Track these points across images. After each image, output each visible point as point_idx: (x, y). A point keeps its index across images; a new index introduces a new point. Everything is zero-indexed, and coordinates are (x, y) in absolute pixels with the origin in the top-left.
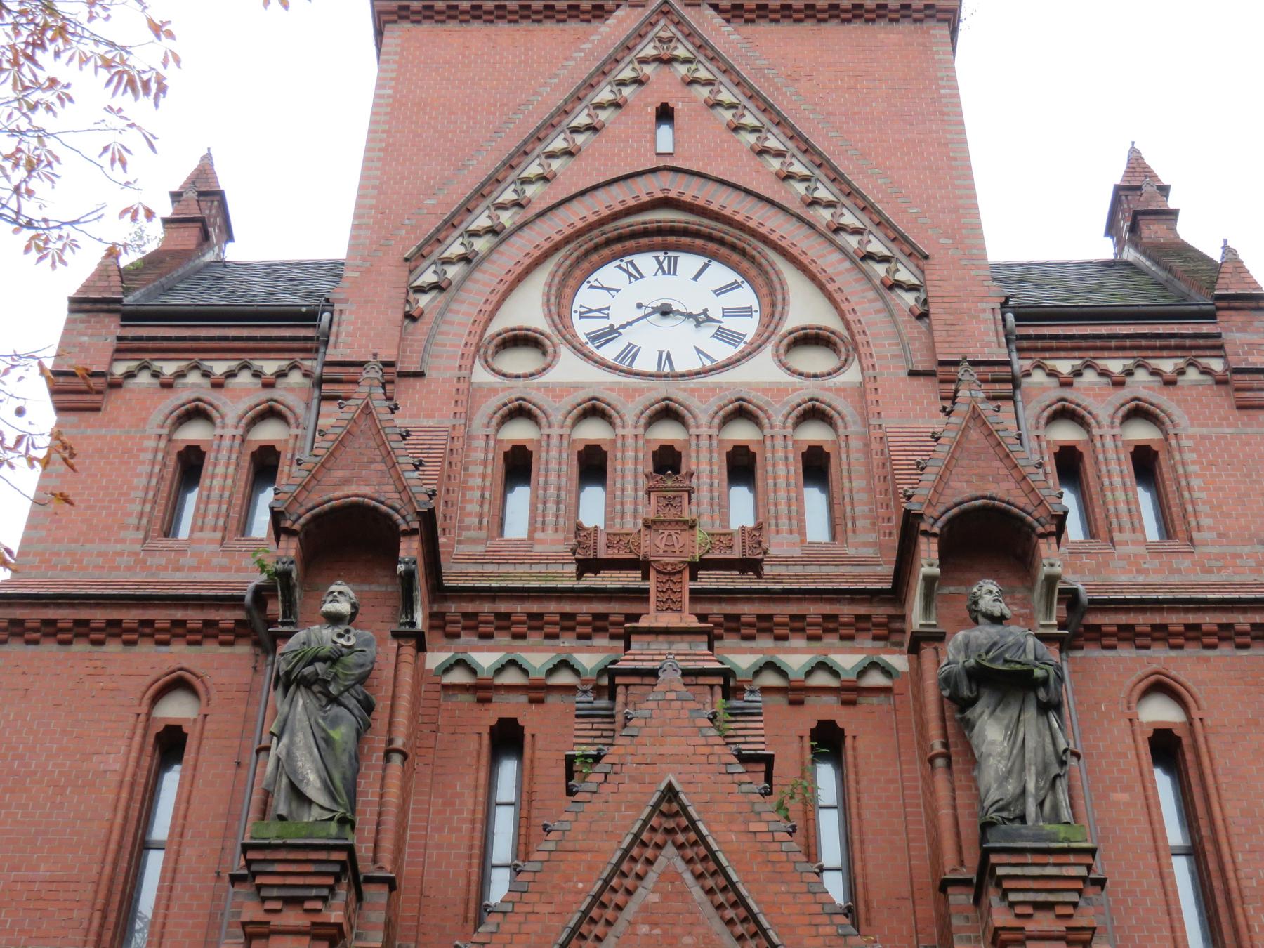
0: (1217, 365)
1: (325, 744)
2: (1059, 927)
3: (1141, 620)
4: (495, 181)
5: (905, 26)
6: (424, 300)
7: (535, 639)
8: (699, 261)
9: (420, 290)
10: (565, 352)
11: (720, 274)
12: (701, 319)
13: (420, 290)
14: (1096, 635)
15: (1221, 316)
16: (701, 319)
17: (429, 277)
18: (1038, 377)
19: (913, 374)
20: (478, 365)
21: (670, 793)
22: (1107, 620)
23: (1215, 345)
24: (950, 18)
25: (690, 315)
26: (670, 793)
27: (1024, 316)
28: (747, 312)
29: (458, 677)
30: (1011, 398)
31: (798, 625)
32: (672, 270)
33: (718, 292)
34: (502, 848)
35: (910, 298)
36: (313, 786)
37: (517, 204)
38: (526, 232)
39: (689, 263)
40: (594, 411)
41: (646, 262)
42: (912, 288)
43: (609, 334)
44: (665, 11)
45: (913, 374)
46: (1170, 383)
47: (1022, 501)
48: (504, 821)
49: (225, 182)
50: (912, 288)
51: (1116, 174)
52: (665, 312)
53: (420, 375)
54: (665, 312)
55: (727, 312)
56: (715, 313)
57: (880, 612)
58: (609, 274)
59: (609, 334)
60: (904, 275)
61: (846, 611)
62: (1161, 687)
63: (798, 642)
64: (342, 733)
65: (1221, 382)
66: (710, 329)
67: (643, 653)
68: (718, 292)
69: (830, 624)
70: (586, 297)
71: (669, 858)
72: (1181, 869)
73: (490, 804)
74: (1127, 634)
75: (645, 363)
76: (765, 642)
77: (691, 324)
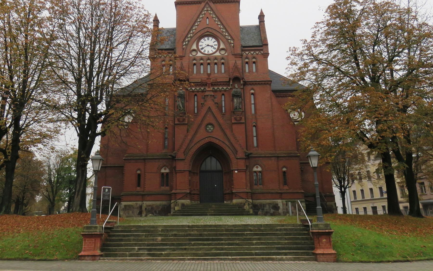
0: (262, 52)
1: (182, 103)
3: (251, 83)
5: (234, 3)
6: (184, 46)
7: (197, 86)
8: (212, 38)
9: (184, 45)
10: (199, 52)
11: (214, 40)
12: (212, 46)
13: (184, 45)
14: (247, 84)
16: (212, 46)
18: (245, 54)
22: (248, 83)
23: (262, 50)
24: (239, 2)
25: (211, 46)
27: (244, 47)
28: (216, 45)
29: (191, 90)
30: (242, 57)
31: (221, 84)
32: (209, 40)
33: (214, 42)
34: (196, 105)
38: (195, 36)
39: (210, 38)
41: (206, 38)
42: (232, 43)
43: (202, 48)
44: (207, 3)
47: (240, 76)
48: (196, 103)
50: (232, 43)
51: (259, 14)
52: (208, 45)
54: (208, 45)
55: (214, 45)
56: (213, 46)
57: (228, 83)
58: (202, 40)
59: (202, 48)
60: (232, 42)
61: (225, 83)
62: (252, 89)
66: (213, 47)
67: (207, 93)
68: (214, 42)
69: (223, 84)
70: (200, 44)
71: (210, 113)
72: (253, 106)
74: (250, 84)
75: (206, 53)
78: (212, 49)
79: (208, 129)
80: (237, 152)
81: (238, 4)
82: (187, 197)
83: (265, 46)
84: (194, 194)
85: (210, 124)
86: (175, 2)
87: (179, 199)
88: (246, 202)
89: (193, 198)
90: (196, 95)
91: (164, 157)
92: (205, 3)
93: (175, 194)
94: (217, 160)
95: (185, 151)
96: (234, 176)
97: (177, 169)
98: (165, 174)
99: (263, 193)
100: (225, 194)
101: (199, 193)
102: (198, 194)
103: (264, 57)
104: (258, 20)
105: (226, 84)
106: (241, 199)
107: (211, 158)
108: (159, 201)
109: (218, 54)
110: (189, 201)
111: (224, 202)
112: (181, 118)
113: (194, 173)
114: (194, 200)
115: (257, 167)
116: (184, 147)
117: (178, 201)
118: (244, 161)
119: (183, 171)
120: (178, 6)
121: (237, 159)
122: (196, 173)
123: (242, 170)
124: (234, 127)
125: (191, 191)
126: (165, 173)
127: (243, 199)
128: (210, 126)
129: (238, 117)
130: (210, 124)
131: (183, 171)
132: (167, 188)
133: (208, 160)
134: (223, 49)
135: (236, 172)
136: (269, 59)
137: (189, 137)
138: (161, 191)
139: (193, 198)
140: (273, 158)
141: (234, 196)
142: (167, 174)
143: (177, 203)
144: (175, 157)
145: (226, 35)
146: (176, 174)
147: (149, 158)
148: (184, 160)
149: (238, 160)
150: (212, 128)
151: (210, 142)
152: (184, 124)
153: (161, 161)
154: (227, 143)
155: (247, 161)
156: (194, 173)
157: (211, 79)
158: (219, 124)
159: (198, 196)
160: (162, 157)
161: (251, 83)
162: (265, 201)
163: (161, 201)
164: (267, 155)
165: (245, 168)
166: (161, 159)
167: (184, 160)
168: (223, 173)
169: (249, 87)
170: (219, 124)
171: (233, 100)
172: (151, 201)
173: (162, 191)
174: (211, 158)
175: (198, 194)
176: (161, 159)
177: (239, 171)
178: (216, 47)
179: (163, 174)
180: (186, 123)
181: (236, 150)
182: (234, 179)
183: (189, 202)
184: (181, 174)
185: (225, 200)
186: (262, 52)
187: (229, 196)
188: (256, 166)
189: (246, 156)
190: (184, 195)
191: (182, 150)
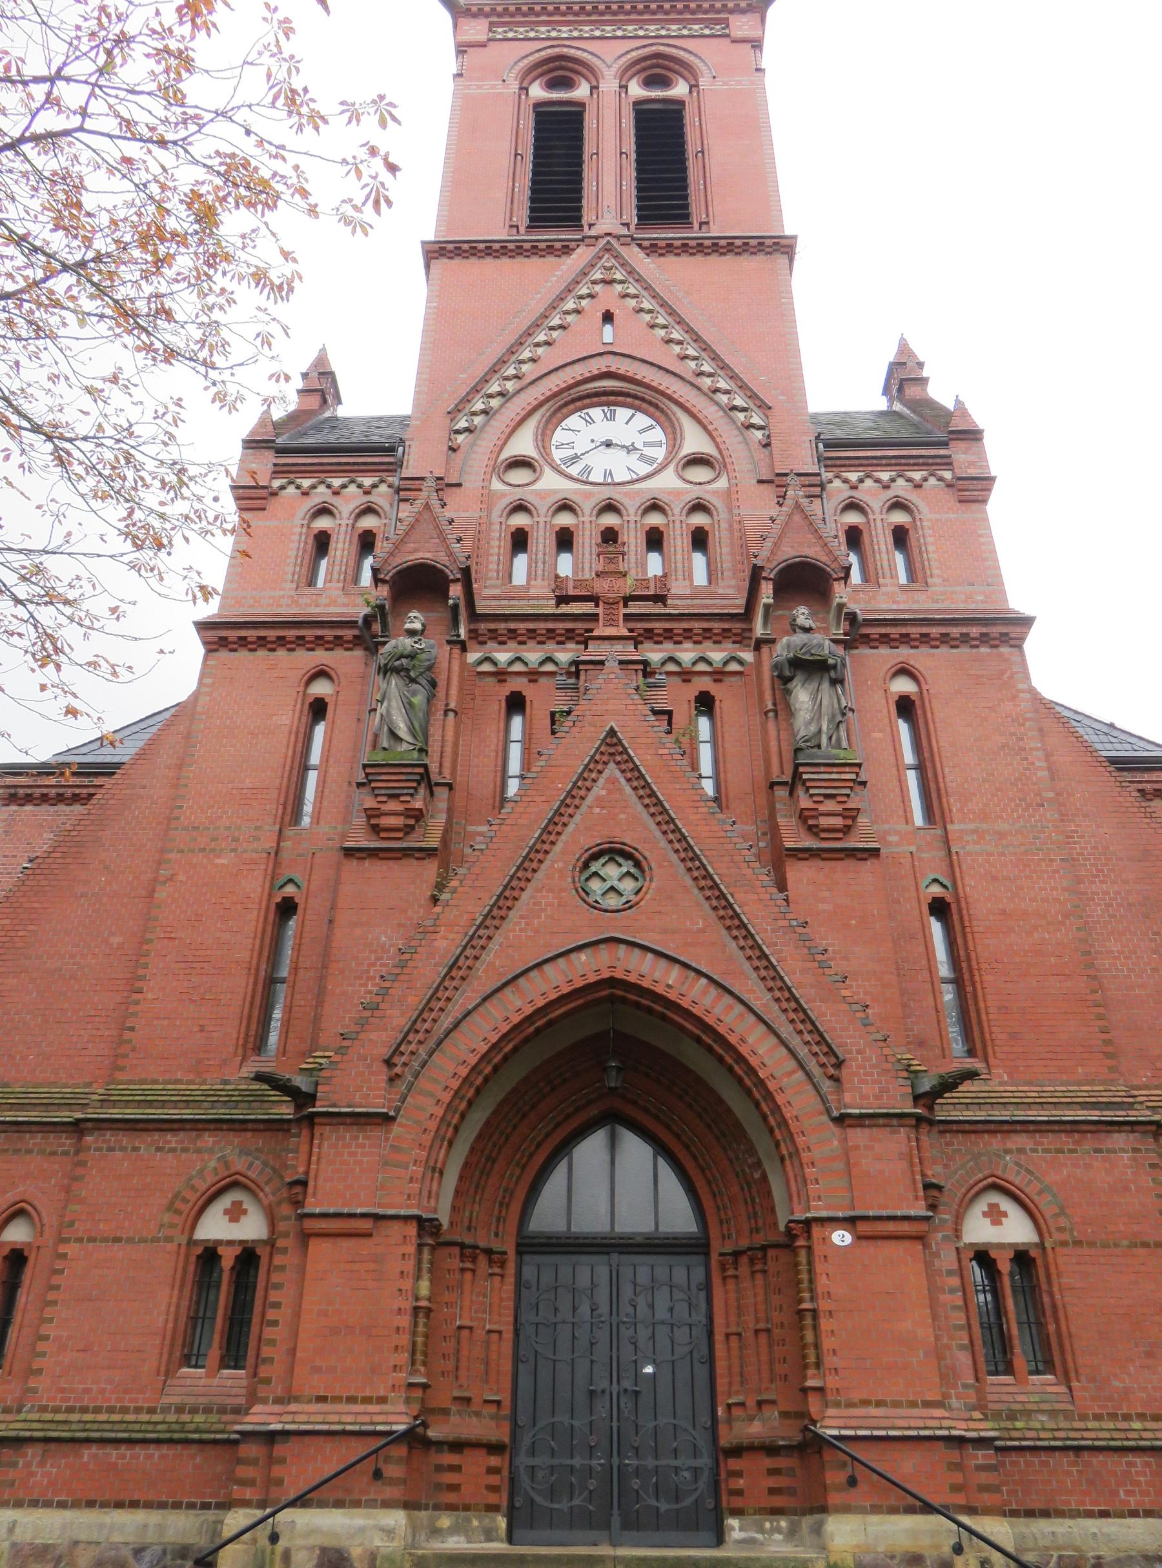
0: (948, 475)
1: (409, 706)
2: (838, 808)
3: (894, 631)
4: (502, 362)
6: (460, 438)
7: (531, 644)
9: (458, 432)
10: (547, 470)
11: (642, 420)
12: (631, 449)
13: (458, 432)
14: (866, 640)
15: (952, 444)
16: (631, 449)
17: (462, 424)
18: (837, 483)
19: (760, 482)
20: (494, 479)
21: (612, 732)
23: (947, 463)
25: (623, 447)
26: (612, 732)
29: (486, 667)
31: (688, 634)
33: (641, 432)
35: (759, 434)
36: (402, 731)
37: (516, 377)
38: (522, 395)
39: (623, 413)
40: (565, 506)
41: (596, 413)
45: (760, 482)
46: (918, 486)
47: (824, 559)
49: (335, 367)
51: (890, 355)
52: (608, 444)
53: (459, 485)
54: (608, 444)
56: (639, 445)
57: (737, 626)
58: (574, 421)
60: (756, 420)
62: (904, 671)
63: (688, 645)
64: (419, 700)
65: (949, 486)
66: (635, 456)
68: (641, 432)
70: (559, 436)
71: (612, 770)
72: (912, 777)
73: (506, 741)
74: (885, 640)
76: (668, 645)
77: (623, 453)
78: (633, 460)
79: (596, 886)
80: (839, 1065)
81: (783, 260)
82: (377, 1474)
83: (962, 445)
84: (457, 1446)
85: (615, 852)
86: (424, 243)
87: (301, 1501)
88: (958, 1549)
89: (454, 1488)
90: (516, 704)
91: (237, 1114)
92: (592, 252)
93: (271, 1437)
94: (662, 1148)
95: (397, 1051)
96: (822, 1282)
97: (313, 1206)
98: (228, 1258)
99: (1078, 1449)
100: (736, 1451)
101: (500, 1433)
102: (494, 1448)
103: (960, 501)
104: (884, 399)
105: (726, 633)
106: (910, 1510)
107: (613, 1144)
108: (134, 1505)
109: (668, 481)
110: (397, 1518)
111: (719, 1539)
112: (393, 806)
113: (468, 1252)
114: (451, 1507)
115: (995, 1216)
116: (398, 1018)
117: (285, 1516)
118: (899, 1140)
119: (366, 1225)
120: (438, 265)
121: (841, 1120)
122: (489, 1252)
123: (891, 1227)
124: (799, 874)
125: (426, 1413)
126: (230, 1243)
127: (928, 1508)
128: (612, 872)
129: (830, 806)
130: (615, 852)
131: (366, 1225)
132: (233, 1380)
133: (592, 1149)
134: (697, 460)
135: (841, 1238)
136: (997, 507)
137: (447, 943)
138: (166, 1410)
139: (454, 1488)
140: (1119, 1140)
141: (835, 1477)
142: (248, 1256)
143: (274, 1538)
144: (311, 1098)
145: (716, 391)
146: (305, 1246)
147: (115, 1113)
148: (386, 1119)
149: (858, 1136)
150: (628, 886)
151: (612, 982)
152: (407, 853)
153: (208, 1140)
154: (760, 998)
155: (923, 1138)
156: (468, 1252)
157: (624, 575)
158: (690, 857)
159: (494, 1461)
160: (222, 1113)
161: (894, 631)
162: (1110, 1526)
163: (148, 1505)
164: (1069, 1115)
165: (919, 1209)
166: (217, 1124)
167: (386, 1119)
168: (714, 1257)
169: (887, 657)
170: (690, 857)
171: (783, 709)
172: (62, 1505)
173: (180, 1410)
174: (613, 1144)
175: (494, 1448)
176: (217, 1124)
177: (862, 1227)
178: (660, 453)
179: (210, 1255)
180: (434, 842)
181: (831, 1052)
182: (823, 1305)
183: (389, 1533)
184: (346, 1244)
185: (737, 1512)
186: (948, 475)
187: (773, 1472)
188: (981, 1206)
189: (917, 1098)
190: (360, 1448)
191: (380, 1041)
